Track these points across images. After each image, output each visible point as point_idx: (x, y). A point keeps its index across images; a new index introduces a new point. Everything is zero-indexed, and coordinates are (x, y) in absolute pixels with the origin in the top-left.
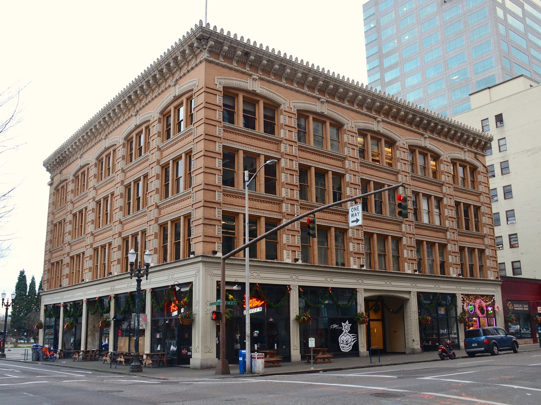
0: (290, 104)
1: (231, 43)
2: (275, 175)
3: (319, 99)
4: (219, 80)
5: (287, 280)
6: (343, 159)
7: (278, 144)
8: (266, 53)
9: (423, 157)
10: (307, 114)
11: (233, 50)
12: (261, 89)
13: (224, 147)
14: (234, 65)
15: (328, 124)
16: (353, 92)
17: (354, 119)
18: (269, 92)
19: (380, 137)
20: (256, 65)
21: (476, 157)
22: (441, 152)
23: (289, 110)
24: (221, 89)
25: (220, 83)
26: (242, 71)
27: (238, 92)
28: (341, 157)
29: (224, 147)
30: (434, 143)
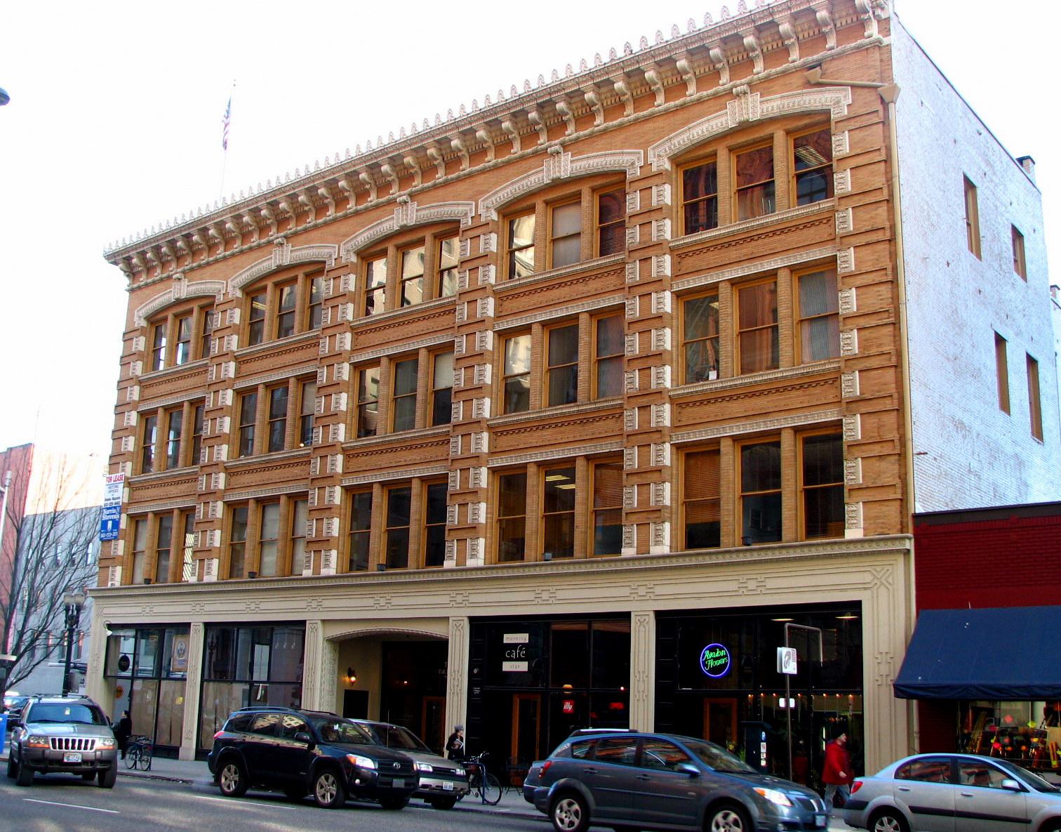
5: (294, 610)
21: (809, 84)
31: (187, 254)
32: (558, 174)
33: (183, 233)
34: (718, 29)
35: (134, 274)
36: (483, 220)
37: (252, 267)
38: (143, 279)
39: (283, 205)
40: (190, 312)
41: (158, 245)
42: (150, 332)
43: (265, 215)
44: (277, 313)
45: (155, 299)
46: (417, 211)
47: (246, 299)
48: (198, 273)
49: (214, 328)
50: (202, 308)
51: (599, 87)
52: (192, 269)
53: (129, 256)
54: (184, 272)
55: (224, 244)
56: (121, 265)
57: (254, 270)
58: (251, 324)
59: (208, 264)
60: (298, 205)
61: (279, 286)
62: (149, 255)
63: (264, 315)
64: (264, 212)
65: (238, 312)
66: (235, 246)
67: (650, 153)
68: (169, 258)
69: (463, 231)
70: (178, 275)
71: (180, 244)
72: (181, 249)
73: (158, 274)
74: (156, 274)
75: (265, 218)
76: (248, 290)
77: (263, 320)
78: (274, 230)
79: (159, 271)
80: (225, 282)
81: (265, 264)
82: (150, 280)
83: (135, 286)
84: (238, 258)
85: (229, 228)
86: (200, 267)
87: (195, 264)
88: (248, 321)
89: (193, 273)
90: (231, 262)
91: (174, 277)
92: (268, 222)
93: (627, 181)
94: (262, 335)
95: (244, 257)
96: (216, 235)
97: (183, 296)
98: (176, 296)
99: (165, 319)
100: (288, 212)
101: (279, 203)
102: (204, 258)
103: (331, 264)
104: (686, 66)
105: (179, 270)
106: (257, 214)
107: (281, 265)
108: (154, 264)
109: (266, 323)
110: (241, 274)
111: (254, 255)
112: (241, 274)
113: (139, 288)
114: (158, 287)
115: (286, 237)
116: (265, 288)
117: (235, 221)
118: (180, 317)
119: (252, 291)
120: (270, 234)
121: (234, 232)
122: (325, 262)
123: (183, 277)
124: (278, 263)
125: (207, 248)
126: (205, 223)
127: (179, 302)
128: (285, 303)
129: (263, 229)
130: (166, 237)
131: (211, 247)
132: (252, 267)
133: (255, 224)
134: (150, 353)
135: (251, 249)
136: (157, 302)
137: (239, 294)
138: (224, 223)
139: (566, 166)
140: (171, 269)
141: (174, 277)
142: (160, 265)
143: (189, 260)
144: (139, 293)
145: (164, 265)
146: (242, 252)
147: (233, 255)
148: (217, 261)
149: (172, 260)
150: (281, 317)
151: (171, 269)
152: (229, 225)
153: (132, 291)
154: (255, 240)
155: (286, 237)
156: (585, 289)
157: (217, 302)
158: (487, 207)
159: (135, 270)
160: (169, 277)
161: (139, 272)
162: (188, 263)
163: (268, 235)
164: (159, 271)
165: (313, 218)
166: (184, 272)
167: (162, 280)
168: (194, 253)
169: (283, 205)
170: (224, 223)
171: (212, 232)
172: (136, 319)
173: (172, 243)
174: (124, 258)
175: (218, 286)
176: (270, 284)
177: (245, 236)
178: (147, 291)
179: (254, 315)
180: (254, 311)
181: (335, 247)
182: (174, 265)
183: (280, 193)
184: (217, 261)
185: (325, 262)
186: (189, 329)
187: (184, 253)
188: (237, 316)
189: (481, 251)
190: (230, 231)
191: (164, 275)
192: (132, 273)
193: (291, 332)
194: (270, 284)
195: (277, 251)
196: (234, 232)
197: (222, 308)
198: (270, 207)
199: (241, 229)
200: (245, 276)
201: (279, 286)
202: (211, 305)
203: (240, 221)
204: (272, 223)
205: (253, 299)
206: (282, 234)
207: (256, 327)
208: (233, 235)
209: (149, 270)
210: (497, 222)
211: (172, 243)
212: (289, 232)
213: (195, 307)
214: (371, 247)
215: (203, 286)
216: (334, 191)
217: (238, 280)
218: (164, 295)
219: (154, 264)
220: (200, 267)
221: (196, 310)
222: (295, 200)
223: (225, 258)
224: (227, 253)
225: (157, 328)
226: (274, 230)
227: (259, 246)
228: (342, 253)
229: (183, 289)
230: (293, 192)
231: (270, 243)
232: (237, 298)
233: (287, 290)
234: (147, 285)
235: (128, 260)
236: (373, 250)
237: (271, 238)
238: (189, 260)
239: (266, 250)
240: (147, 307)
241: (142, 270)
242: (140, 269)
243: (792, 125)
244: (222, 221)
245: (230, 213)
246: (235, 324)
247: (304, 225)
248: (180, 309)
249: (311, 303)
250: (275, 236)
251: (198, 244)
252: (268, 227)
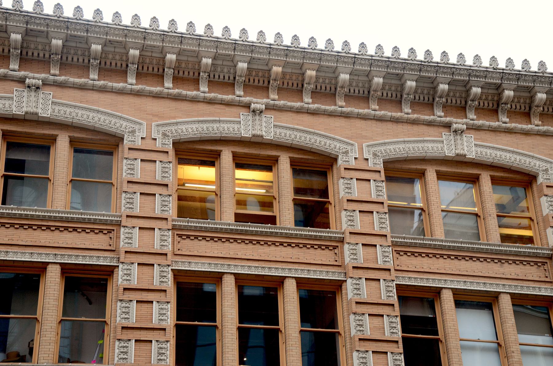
0: (361, 149)
1: (27, 23)
2: (333, 323)
3: (448, 126)
4: (162, 129)
6: (111, 227)
7: (335, 247)
8: (310, 55)
9: (523, 189)
10: (419, 167)
11: (230, 64)
12: (479, 150)
13: (177, 274)
14: (439, 114)
15: (485, 179)
16: (286, 65)
17: (366, 138)
18: (205, 126)
19: (273, 153)
20: (258, 82)
22: (533, 162)
23: (363, 166)
24: (381, 167)
25: (375, 155)
26: (522, 129)
27: (423, 167)
28: (105, 222)
29: (177, 274)
30: (68, 97)
139: (268, 128)
156: (502, 270)
236: (398, 166)
243: (240, 150)
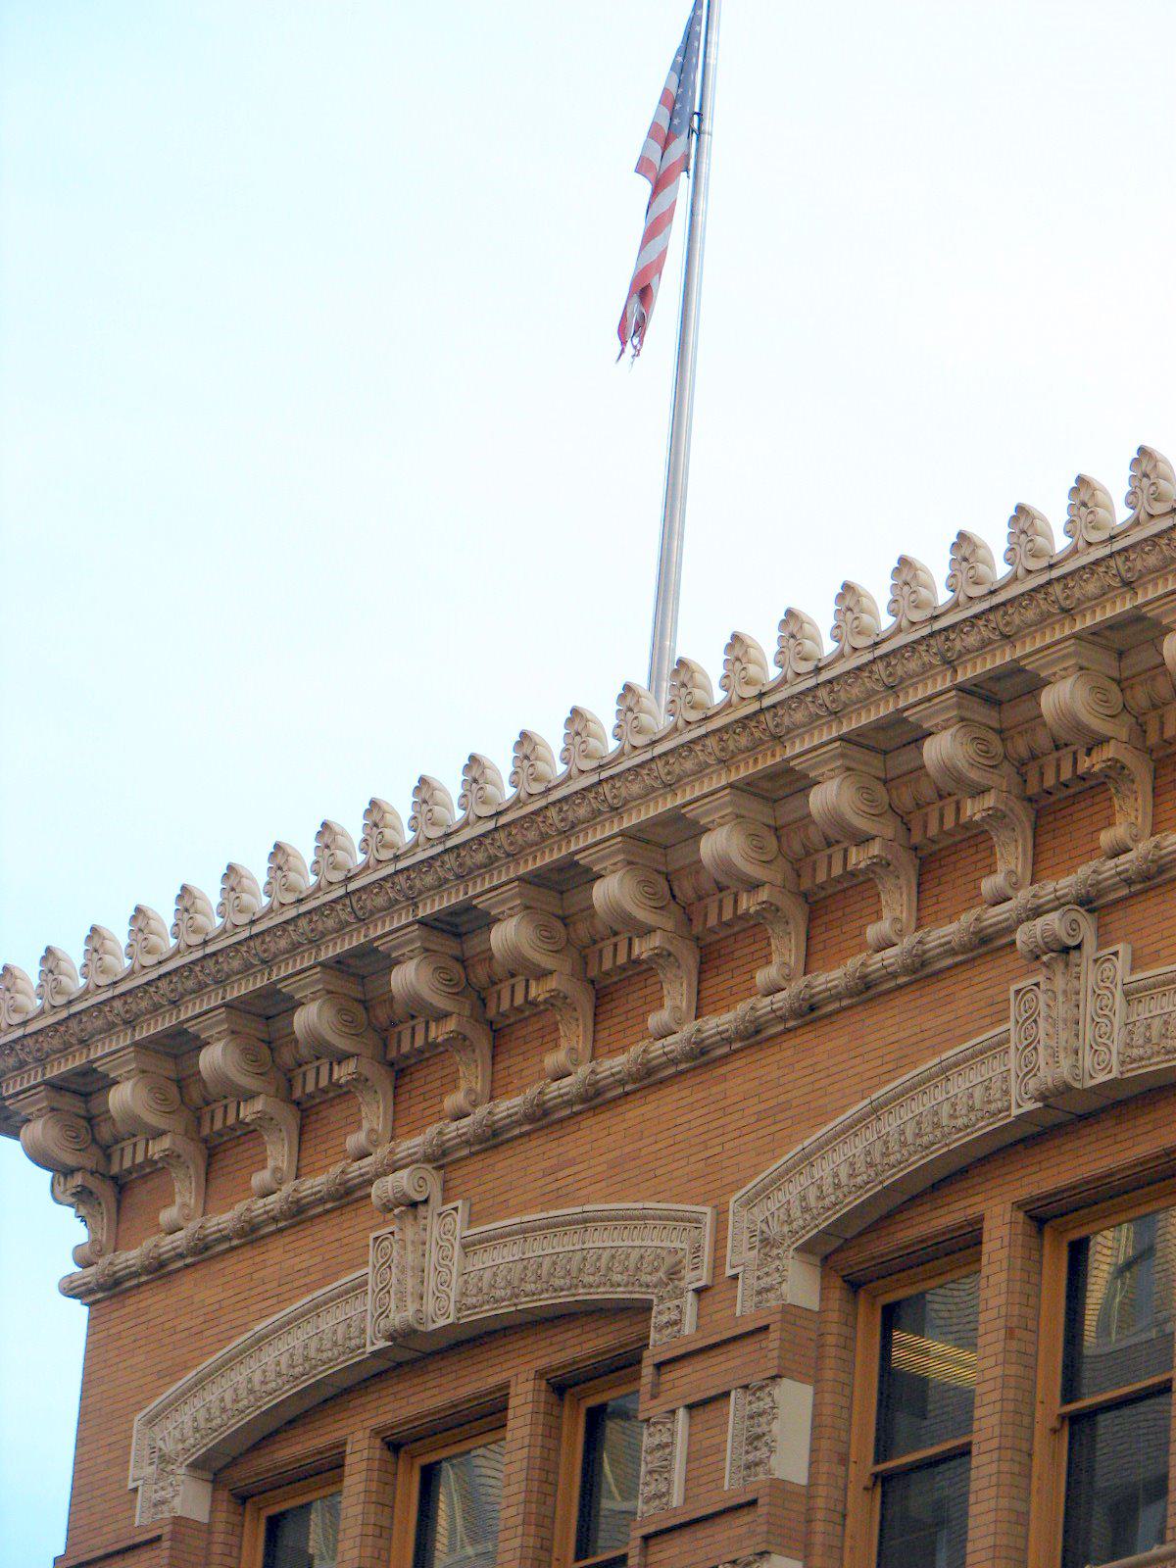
31: (459, 1040)
32: (1064, 1070)
33: (426, 910)
34: (553, 812)
35: (121, 1186)
36: (744, 1308)
37: (876, 1111)
38: (180, 1214)
39: (1064, 697)
40: (486, 1416)
41: (270, 993)
42: (848, 1344)
43: (948, 769)
44: (1050, 1406)
45: (259, 1342)
46: (467, 1247)
47: (236, 1530)
48: (536, 1156)
49: (647, 1513)
50: (560, 1386)
51: (458, 935)
52: (492, 1140)
53: (87, 1072)
54: (440, 1159)
55: (690, 960)
56: (36, 1130)
57: (890, 1124)
58: (885, 1482)
59: (595, 1100)
60: (1043, 741)
61: (1060, 1223)
62: (215, 1058)
63: (966, 1423)
64: (942, 749)
65: (794, 1404)
66: (763, 976)
67: (739, 1222)
68: (343, 1073)
69: (659, 1366)
70: (401, 1181)
71: (408, 977)
72: (418, 1010)
73: (273, 1174)
74: (260, 1178)
75: (953, 787)
76: (858, 1258)
77: (965, 1452)
78: (1011, 858)
79: (278, 1154)
80: (709, 1213)
81: (329, 1322)
82: (223, 1220)
83: (131, 1257)
84: (788, 1050)
85: (725, 864)
86: (542, 1119)
87: (508, 1106)
88: (864, 1465)
89: (503, 1166)
90: (740, 1080)
91: (383, 1189)
92: (973, 810)
93: (650, 1357)
94: (961, 1541)
95: (827, 1047)
96: (643, 915)
97: (441, 1312)
98: (397, 1319)
99: (330, 1468)
100: (1099, 741)
101: (1035, 686)
102: (566, 1062)
103: (680, 1320)
104: (962, 764)
105: (412, 1144)
106: (902, 761)
107: (1065, 1090)
108: (248, 1112)
109: (985, 1471)
110: (807, 1158)
111: (889, 1026)
112: (807, 1158)
113: (159, 1270)
114: (279, 1257)
115: (1087, 902)
116: (966, 1243)
117: (759, 812)
118: (421, 1455)
119: (885, 1263)
120: (988, 885)
121: (754, 886)
122: (644, 1309)
123: (433, 1187)
124: (1048, 1075)
125: (584, 1001)
126: (570, 830)
127: (412, 1355)
128: (1103, 1329)
129: (938, 860)
130: (315, 942)
131: (610, 992)
132: (876, 1111)
133: (887, 828)
134: (1041, 1443)
135: (867, 991)
136: (272, 1356)
137: (801, 1286)
138: (684, 828)
140: (355, 1140)
141: (383, 1189)
142: (288, 1118)
143: (472, 1077)
144: (155, 1302)
145: (309, 1115)
146: (809, 1013)
147: (754, 1037)
148: (648, 1079)
149: (360, 1080)
150: (1079, 1424)
151: (355, 1140)
152: (721, 844)
153: (102, 1290)
154: (892, 930)
155: (1087, 902)
157: (659, 1344)
158: (766, 1242)
159: (128, 1158)
160: (348, 1196)
161: (153, 1170)
162: (465, 1099)
163: (974, 898)
164: (278, 1154)
165: (583, 1045)
166: (440, 1159)
167: (298, 1215)
168: (502, 1028)
169: (1064, 697)
170: (684, 828)
171: (612, 890)
172: (139, 1471)
173: (358, 975)
174: (56, 1086)
175: (655, 1240)
176: (357, 1442)
177: (827, 908)
178: (201, 1291)
179: (903, 1422)
180: (900, 1396)
181: (696, 1221)
182: (374, 1115)
183: (1043, 621)
184: (648, 1079)
185: (644, 1309)
186: (479, 1526)
187: (438, 1032)
188: (790, 1432)
189: (731, 1485)
190: (729, 882)
191: (316, 1183)
192: (100, 1175)
193: (1147, 1518)
194: (357, 1442)
195: (1044, 996)
196: (754, 886)
197: (692, 1381)
198: (983, 714)
199: (799, 864)
200: (838, 1165)
201: (1060, 1223)
202: (624, 1364)
203: (789, 811)
204: (996, 816)
205: (891, 1317)
206: (1066, 884)
207: (919, 1499)
208: (748, 903)
209: (219, 1151)
210: (208, 1529)
211: (358, 975)
212: (452, 1129)
213: (520, 1377)
214: (888, 1219)
215: (565, 1244)
216: (905, 798)
217: (791, 1192)
218: (316, 1308)
219: (248, 1112)
220: (542, 1119)
221: (525, 1401)
222: (1023, 710)
223: (701, 1058)
224: (717, 1023)
225: (274, 1525)
226: (1011, 858)
227: (921, 972)
228: (740, 1256)
229: (436, 1270)
230: (885, 710)
231: (987, 945)
232: (790, 1312)
233: (1108, 1249)
234: (203, 1252)
235: (82, 1091)
237: (356, 1169)
238: (472, 1077)
239: (326, 1232)
240: (212, 1395)
241: (170, 1156)
242: (157, 1149)
244: (675, 818)
245: (724, 763)
246: (779, 1486)
247: (853, 963)
248: (423, 1402)
249: (1070, 1392)
250: (1023, 897)
251: (523, 969)
252: (976, 840)
